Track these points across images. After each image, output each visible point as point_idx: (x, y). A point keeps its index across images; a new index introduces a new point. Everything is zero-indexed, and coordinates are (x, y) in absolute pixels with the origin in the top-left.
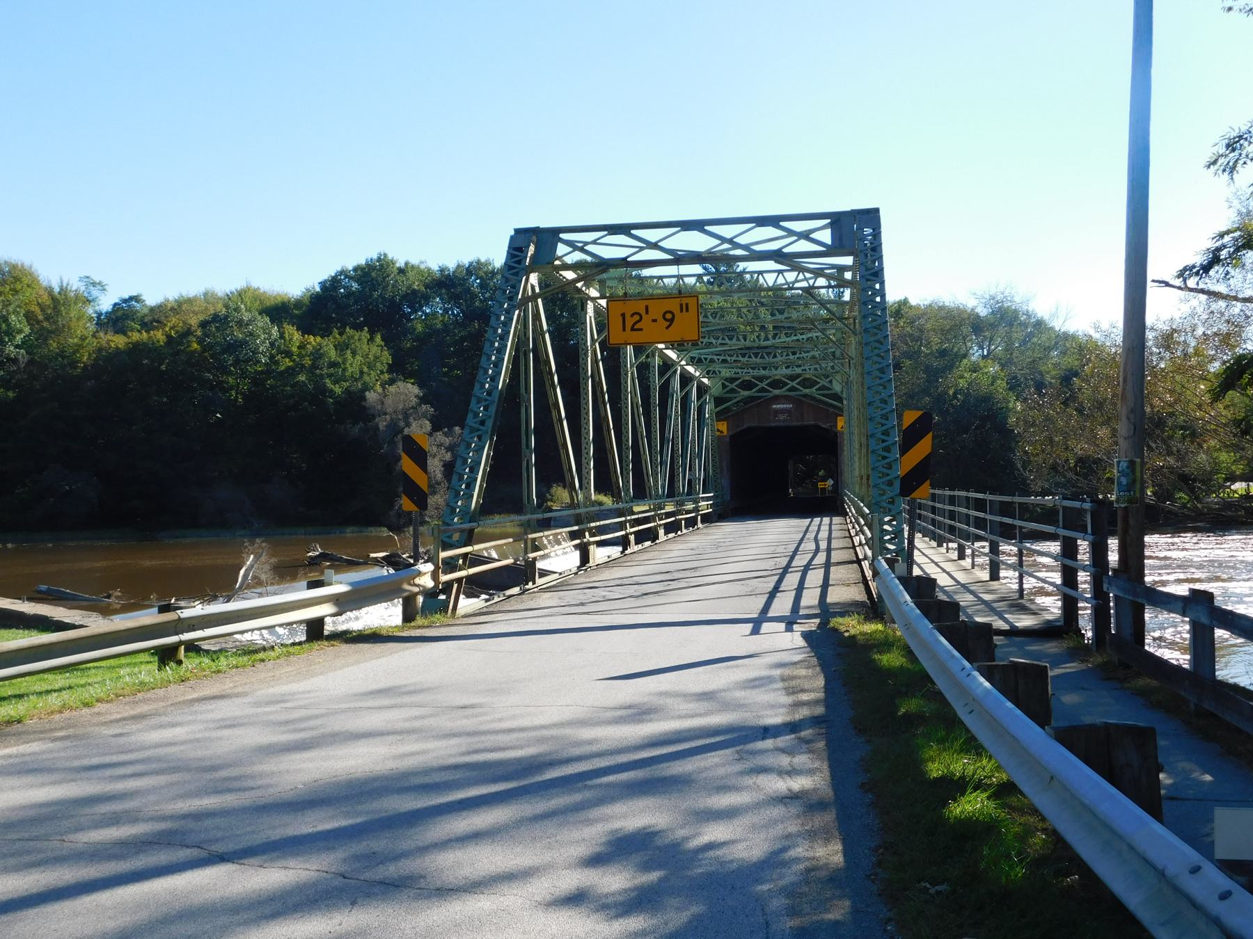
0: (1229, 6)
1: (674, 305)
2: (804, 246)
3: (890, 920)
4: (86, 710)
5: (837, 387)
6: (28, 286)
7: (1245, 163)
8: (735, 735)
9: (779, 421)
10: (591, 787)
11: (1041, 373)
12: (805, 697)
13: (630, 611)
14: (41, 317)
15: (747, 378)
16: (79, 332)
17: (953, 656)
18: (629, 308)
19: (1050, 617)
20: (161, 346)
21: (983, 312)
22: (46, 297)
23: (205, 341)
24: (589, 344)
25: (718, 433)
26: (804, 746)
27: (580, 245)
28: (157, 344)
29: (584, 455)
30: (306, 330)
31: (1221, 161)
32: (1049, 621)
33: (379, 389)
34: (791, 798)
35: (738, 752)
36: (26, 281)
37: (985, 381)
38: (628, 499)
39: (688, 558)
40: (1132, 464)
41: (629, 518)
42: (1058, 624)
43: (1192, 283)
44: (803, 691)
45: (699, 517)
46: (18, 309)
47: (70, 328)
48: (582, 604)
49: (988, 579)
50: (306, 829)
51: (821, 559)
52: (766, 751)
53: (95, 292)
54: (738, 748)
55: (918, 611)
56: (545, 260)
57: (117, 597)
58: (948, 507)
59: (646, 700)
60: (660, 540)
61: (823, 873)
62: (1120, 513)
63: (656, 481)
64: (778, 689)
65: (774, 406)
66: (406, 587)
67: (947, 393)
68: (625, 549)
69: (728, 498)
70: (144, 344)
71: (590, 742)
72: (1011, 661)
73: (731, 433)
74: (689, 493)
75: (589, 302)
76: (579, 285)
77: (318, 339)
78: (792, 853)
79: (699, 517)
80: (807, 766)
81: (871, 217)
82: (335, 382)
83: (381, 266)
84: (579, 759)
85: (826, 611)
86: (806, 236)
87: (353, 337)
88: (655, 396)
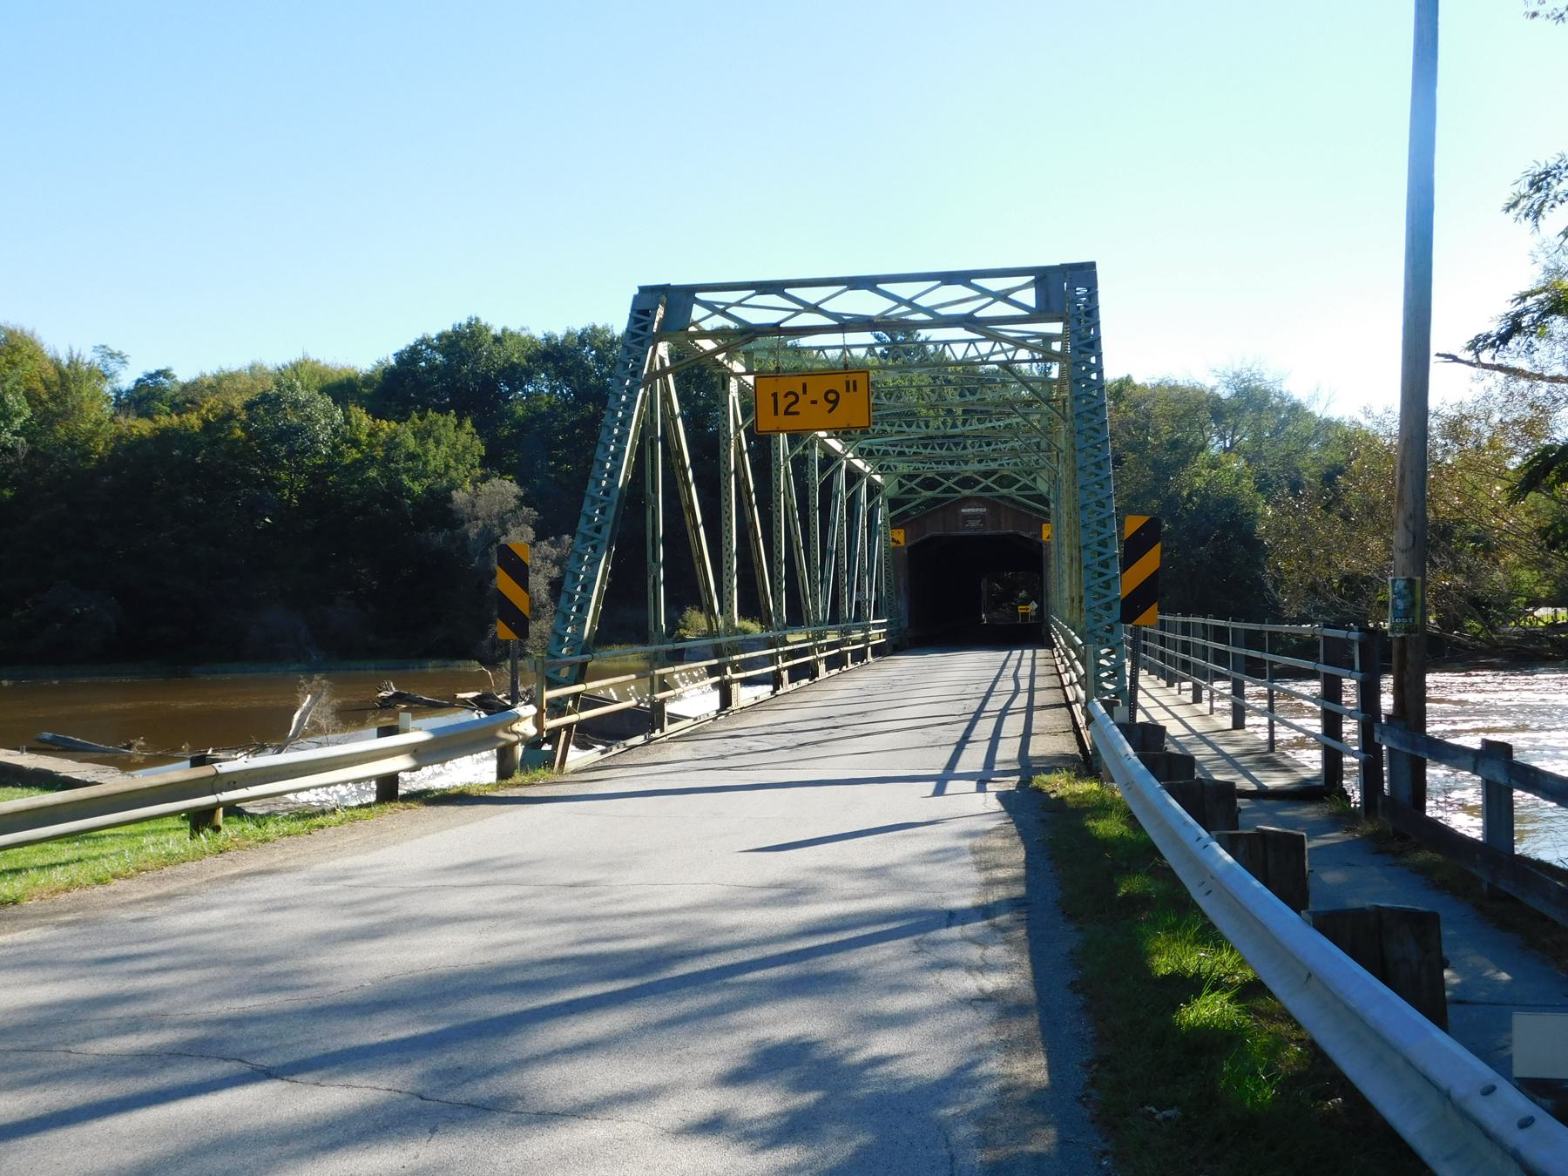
0: (1533, 10)
1: (838, 383)
2: (1001, 309)
3: (1105, 1153)
4: (99, 889)
5: (1042, 487)
6: (29, 357)
7: (1553, 206)
8: (914, 921)
9: (969, 528)
10: (733, 986)
11: (1297, 470)
12: (1000, 874)
13: (783, 766)
14: (45, 397)
15: (930, 475)
16: (92, 415)
17: (1186, 823)
18: (783, 386)
19: (1307, 775)
20: (196, 433)
21: (1225, 393)
22: (51, 371)
23: (251, 427)
24: (732, 431)
25: (893, 544)
26: (999, 935)
27: (721, 307)
28: (192, 431)
29: (725, 571)
30: (377, 413)
31: (1523, 203)
32: (1307, 780)
33: (470, 489)
34: (983, 1000)
35: (916, 943)
36: (26, 351)
37: (1227, 480)
38: (780, 625)
39: (856, 700)
40: (1410, 583)
41: (781, 649)
42: (1318, 783)
43: (1486, 357)
44: (998, 866)
45: (869, 649)
46: (17, 387)
47: (81, 411)
48: (722, 757)
49: (1230, 727)
50: (374, 1038)
51: (1021, 701)
52: (952, 941)
53: (113, 365)
54: (917, 937)
55: (1142, 767)
56: (677, 326)
57: (140, 748)
58: (1180, 637)
59: (801, 877)
60: (820, 678)
61: (1021, 1095)
62: (1395, 645)
63: (815, 604)
64: (967, 864)
65: (963, 510)
66: (502, 735)
67: (1179, 494)
68: (776, 688)
69: (905, 624)
70: (174, 430)
71: (731, 930)
72: (1258, 829)
73: (909, 544)
74: (857, 619)
75: (732, 379)
76: (720, 357)
77: (393, 425)
78: (983, 1069)
79: (869, 649)
80: (1002, 961)
81: (1085, 273)
82: (414, 479)
83: (472, 333)
84: (718, 950)
85: (1027, 766)
86: (1003, 296)
87: (436, 422)
88: (815, 497)
